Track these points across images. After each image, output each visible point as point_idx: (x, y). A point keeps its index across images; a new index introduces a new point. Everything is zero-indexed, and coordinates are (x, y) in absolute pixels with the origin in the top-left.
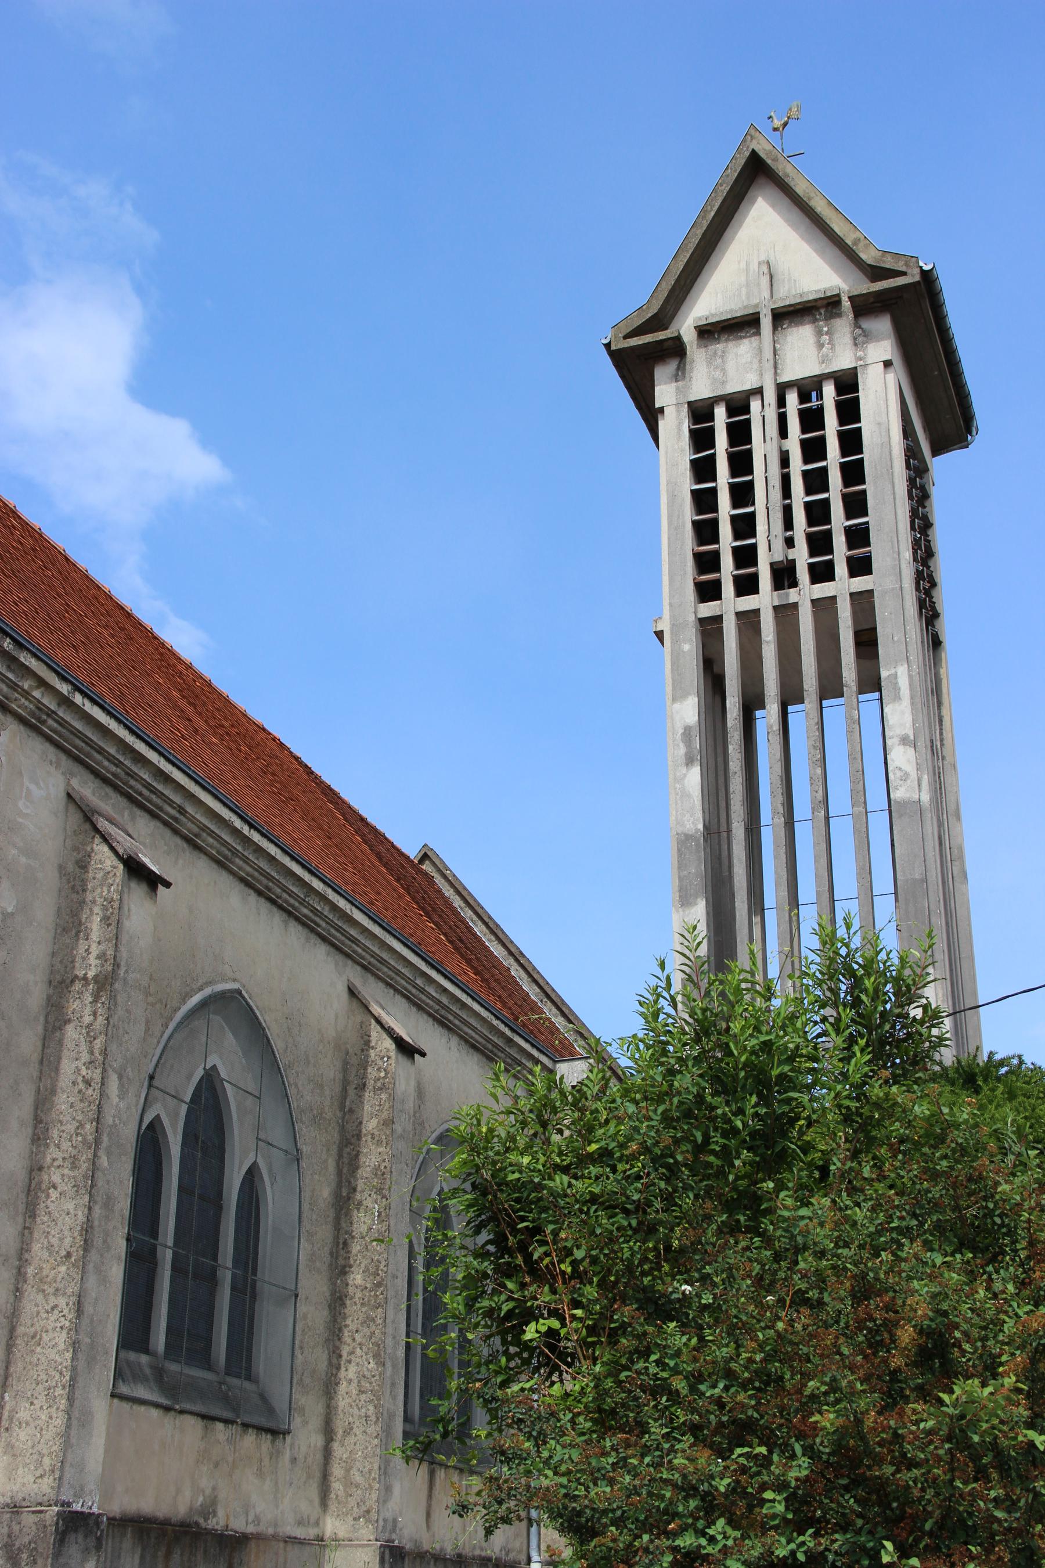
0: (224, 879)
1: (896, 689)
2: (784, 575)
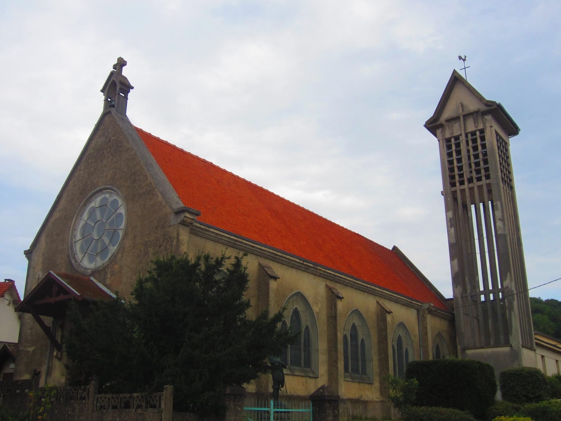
0: (352, 289)
1: (497, 207)
2: (470, 180)
